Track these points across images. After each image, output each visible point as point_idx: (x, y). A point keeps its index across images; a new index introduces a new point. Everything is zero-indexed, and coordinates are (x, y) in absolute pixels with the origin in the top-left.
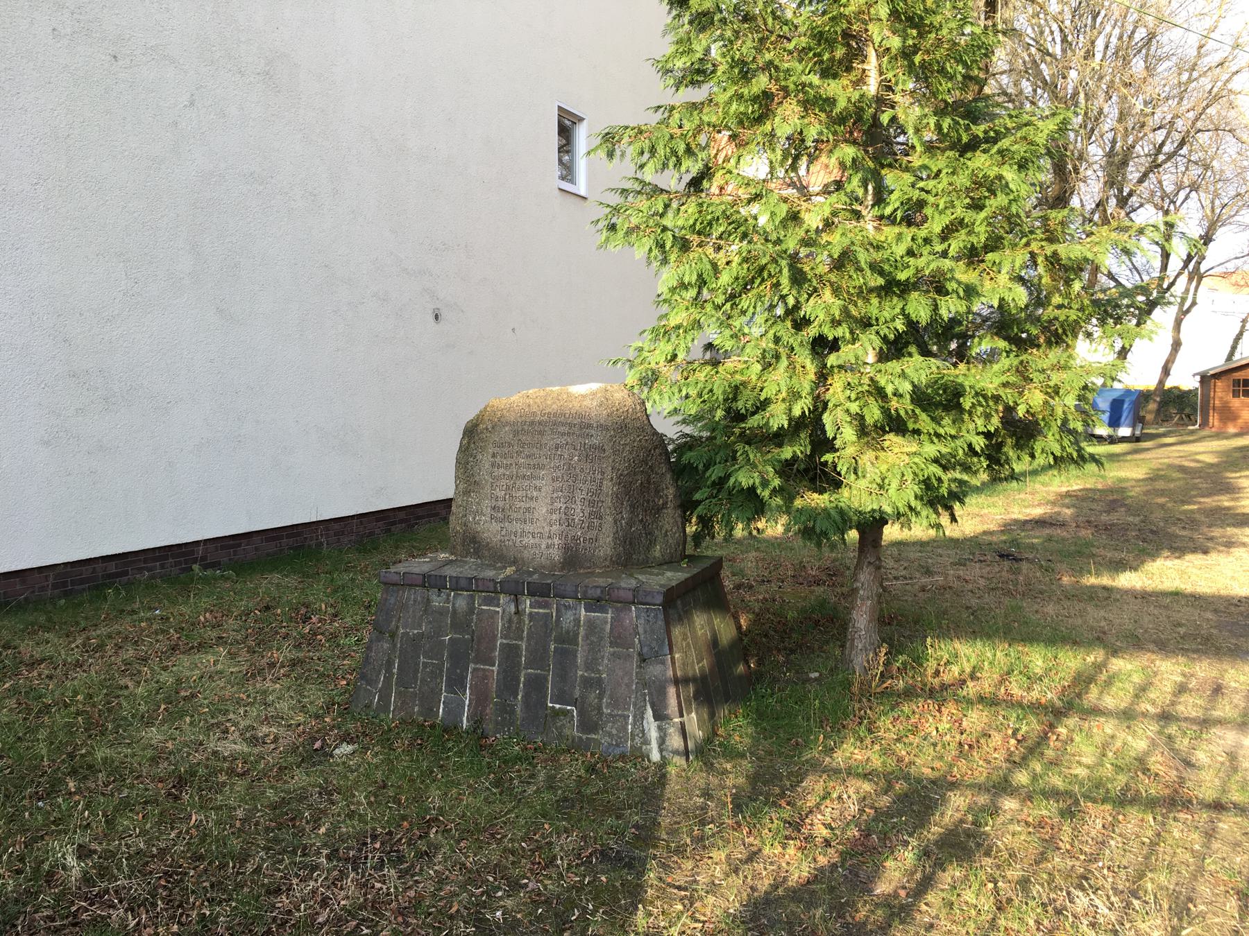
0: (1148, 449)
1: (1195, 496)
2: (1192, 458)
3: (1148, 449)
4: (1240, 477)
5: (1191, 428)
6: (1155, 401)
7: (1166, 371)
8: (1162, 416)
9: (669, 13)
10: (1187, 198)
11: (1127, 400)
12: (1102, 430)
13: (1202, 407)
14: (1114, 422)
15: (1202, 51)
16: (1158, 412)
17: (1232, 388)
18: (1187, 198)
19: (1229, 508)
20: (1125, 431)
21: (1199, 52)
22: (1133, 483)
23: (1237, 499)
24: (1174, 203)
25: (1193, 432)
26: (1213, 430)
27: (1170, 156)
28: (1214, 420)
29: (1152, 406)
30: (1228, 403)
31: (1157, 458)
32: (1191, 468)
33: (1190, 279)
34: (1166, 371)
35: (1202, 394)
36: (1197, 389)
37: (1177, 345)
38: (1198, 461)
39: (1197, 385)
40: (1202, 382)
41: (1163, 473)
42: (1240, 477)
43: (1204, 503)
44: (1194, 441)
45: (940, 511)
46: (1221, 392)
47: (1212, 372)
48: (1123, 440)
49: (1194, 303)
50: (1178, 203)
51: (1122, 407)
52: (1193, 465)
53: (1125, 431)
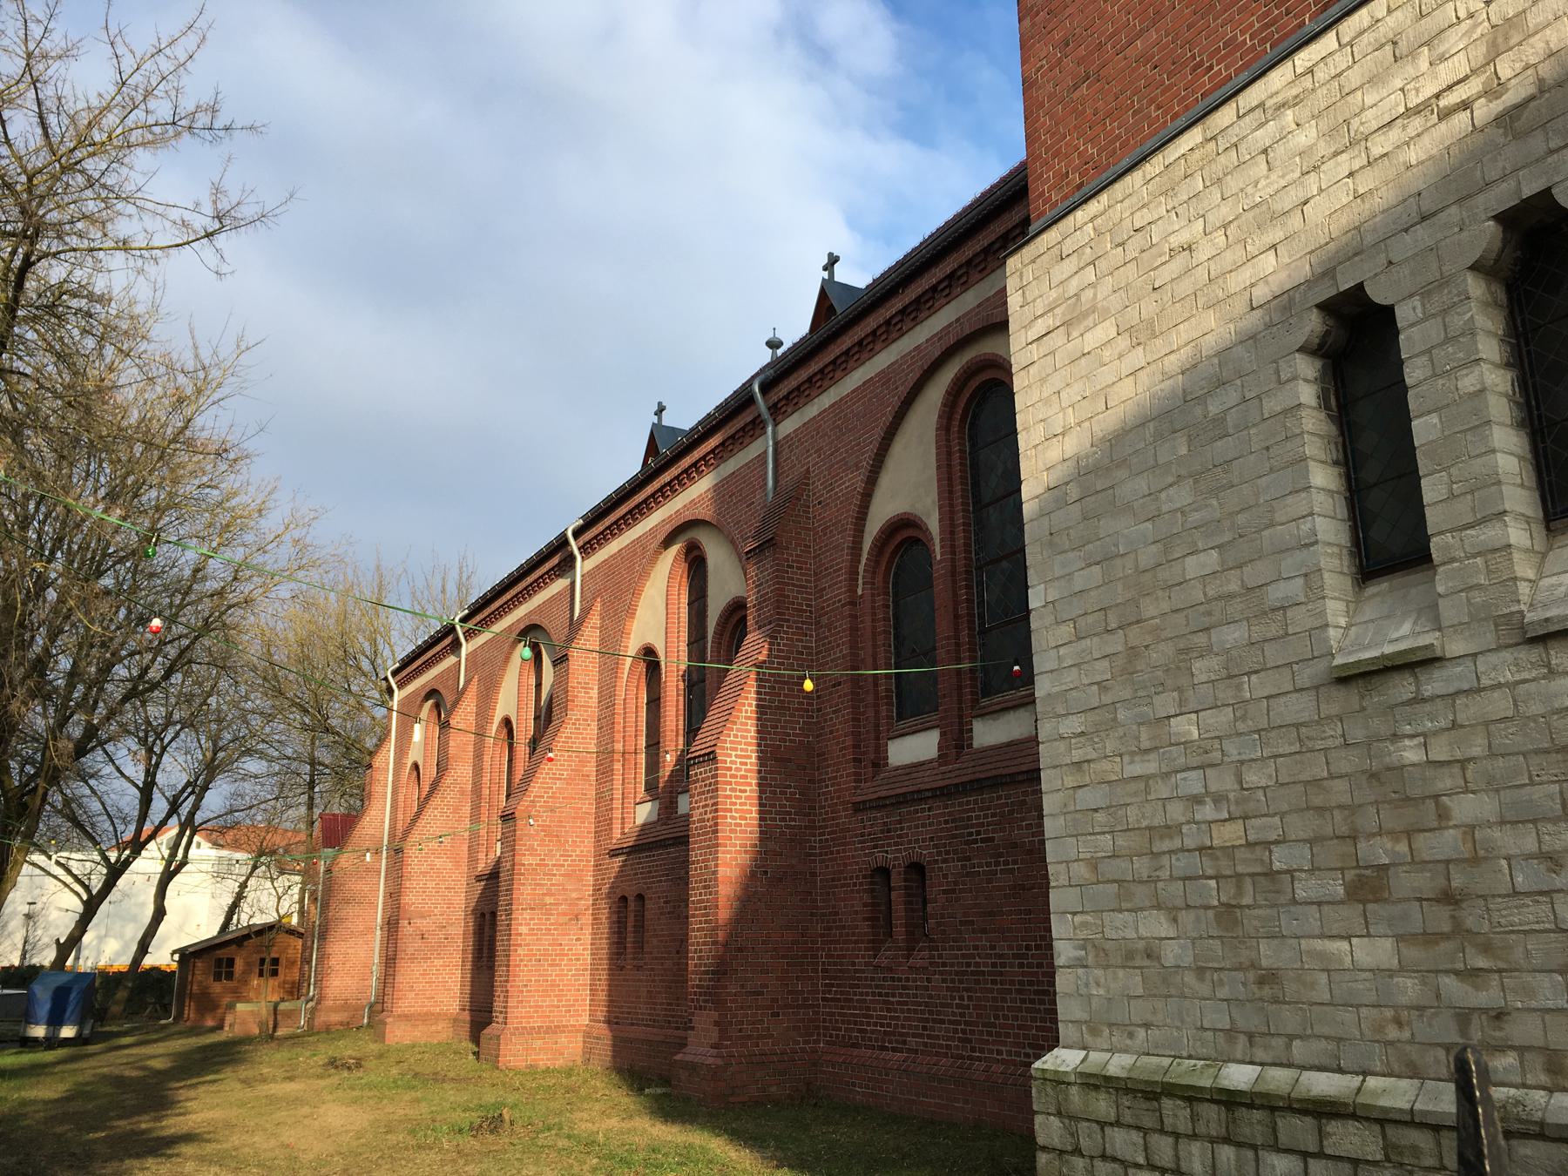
0: (95, 1054)
1: (112, 1119)
2: (140, 1064)
3: (95, 1054)
4: (181, 1088)
5: (163, 1022)
6: (126, 987)
7: (143, 947)
8: (134, 1007)
9: (275, 507)
10: (177, 735)
11: (76, 986)
12: (39, 1031)
13: (178, 993)
14: (55, 1021)
15: (199, 575)
16: (129, 1000)
17: (213, 969)
18: (177, 735)
19: (143, 1132)
20: (68, 1032)
21: (194, 576)
22: (40, 1106)
23: (159, 1119)
24: (162, 740)
25: (165, 1027)
26: (188, 1024)
27: (155, 686)
28: (190, 1012)
29: (122, 994)
30: (207, 988)
31: (94, 1068)
32: (131, 1078)
33: (183, 828)
34: (143, 947)
35: (180, 978)
36: (173, 972)
37: (160, 914)
38: (144, 1068)
39: (174, 966)
40: (180, 962)
41: (89, 1088)
42: (181, 1088)
43: (119, 1127)
44: (155, 1041)
45: (176, 1151)
46: (201, 973)
47: (191, 950)
48: (67, 1042)
49: (184, 863)
50: (166, 741)
51: (68, 996)
52: (135, 1073)
53: (68, 1032)
